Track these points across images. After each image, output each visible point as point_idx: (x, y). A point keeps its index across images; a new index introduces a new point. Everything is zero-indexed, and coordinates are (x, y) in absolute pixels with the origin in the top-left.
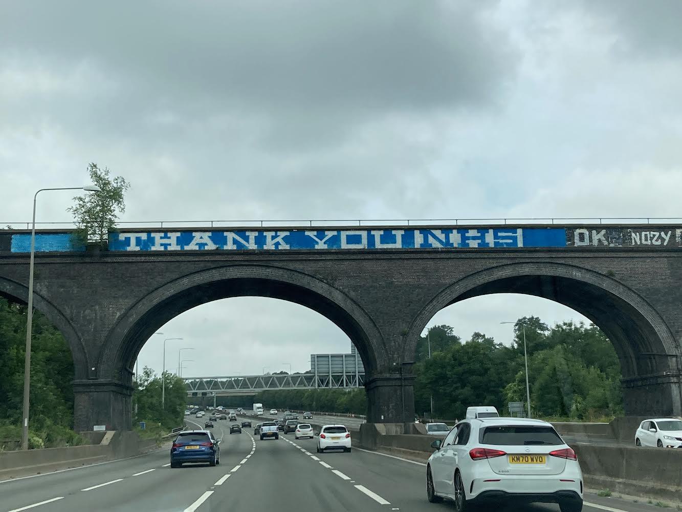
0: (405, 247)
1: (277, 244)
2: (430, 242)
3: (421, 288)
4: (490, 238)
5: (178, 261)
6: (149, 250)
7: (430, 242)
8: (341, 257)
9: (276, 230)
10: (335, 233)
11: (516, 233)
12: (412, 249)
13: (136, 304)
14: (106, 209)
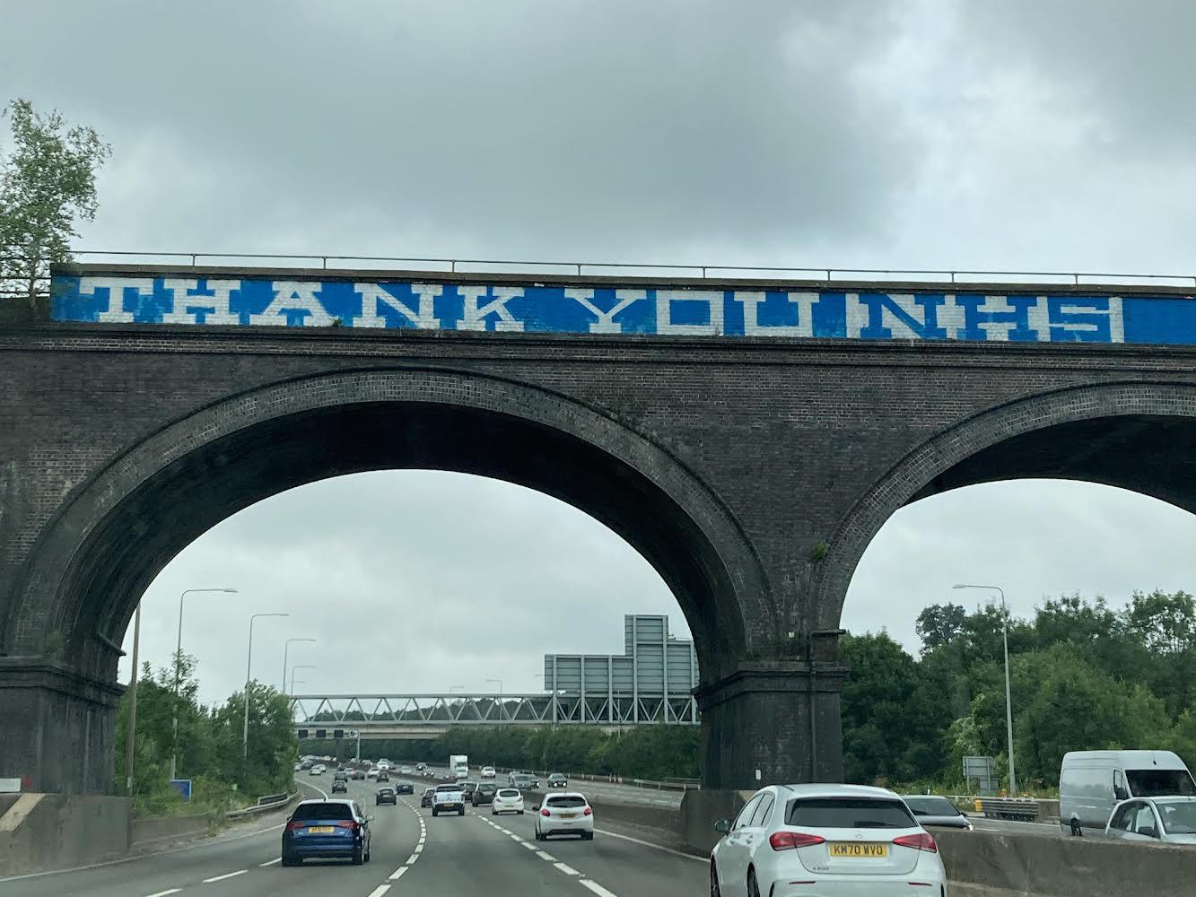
0: (819, 335)
1: (492, 318)
2: (885, 325)
3: (862, 440)
4: (1039, 319)
5: (232, 354)
6: (157, 321)
7: (885, 325)
8: (654, 354)
9: (491, 282)
10: (641, 295)
11: (1107, 308)
12: (840, 340)
13: (116, 461)
14: (44, 209)
